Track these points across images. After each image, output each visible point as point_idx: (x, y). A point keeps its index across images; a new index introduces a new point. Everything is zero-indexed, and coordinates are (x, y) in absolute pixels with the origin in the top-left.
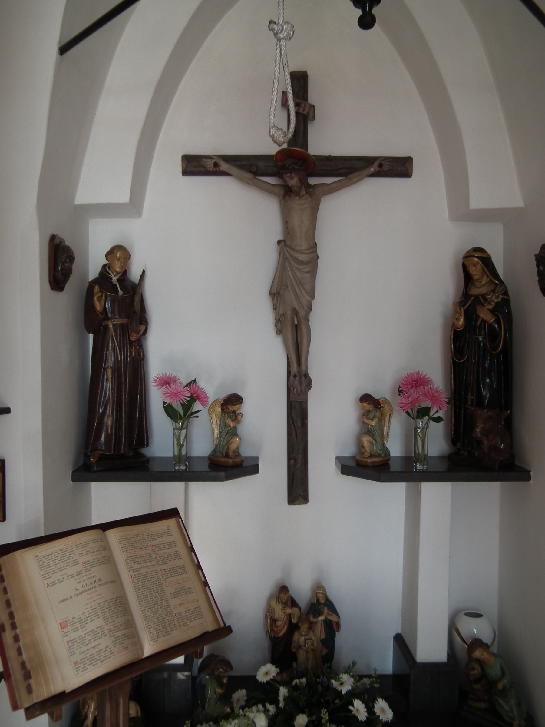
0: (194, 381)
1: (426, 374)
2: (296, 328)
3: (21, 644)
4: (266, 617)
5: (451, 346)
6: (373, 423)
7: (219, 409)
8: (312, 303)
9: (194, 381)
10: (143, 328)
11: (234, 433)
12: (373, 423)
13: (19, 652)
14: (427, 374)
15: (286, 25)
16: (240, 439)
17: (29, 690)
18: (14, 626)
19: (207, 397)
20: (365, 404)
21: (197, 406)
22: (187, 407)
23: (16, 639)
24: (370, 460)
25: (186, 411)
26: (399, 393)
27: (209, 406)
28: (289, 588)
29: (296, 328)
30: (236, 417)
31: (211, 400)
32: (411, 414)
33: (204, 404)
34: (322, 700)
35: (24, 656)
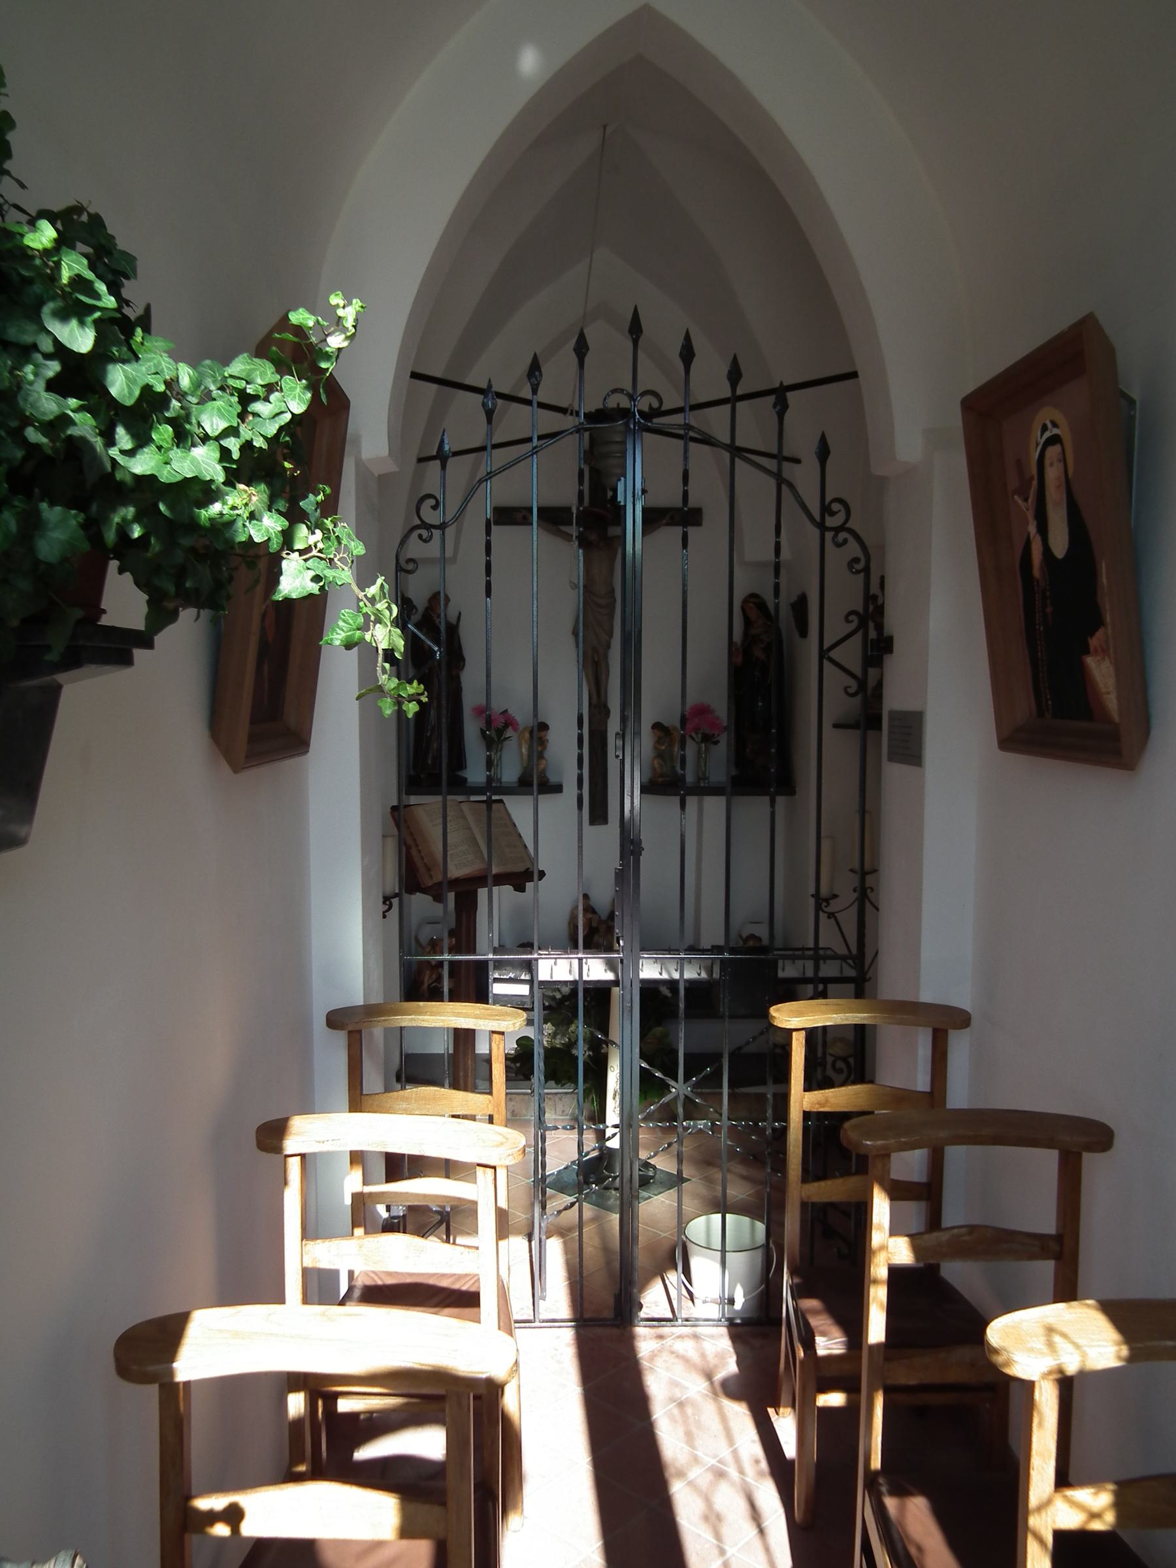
0: (506, 711)
1: (27, 188)
2: (596, 665)
3: (423, 854)
4: (569, 923)
5: (579, 606)
6: (663, 748)
7: (527, 735)
8: (610, 643)
9: (506, 711)
10: (462, 664)
11: (541, 756)
12: (663, 748)
13: (422, 858)
14: (26, 190)
15: (606, 1249)
16: (547, 761)
17: (431, 876)
18: (417, 846)
19: (517, 724)
20: (656, 731)
21: (509, 732)
22: (500, 732)
23: (420, 852)
24: (660, 779)
25: (499, 739)
26: (345, 334)
27: (519, 731)
28: (590, 896)
29: (596, 665)
30: (543, 742)
31: (521, 728)
32: (696, 739)
33: (515, 729)
34: (581, 508)
35: (425, 861)
